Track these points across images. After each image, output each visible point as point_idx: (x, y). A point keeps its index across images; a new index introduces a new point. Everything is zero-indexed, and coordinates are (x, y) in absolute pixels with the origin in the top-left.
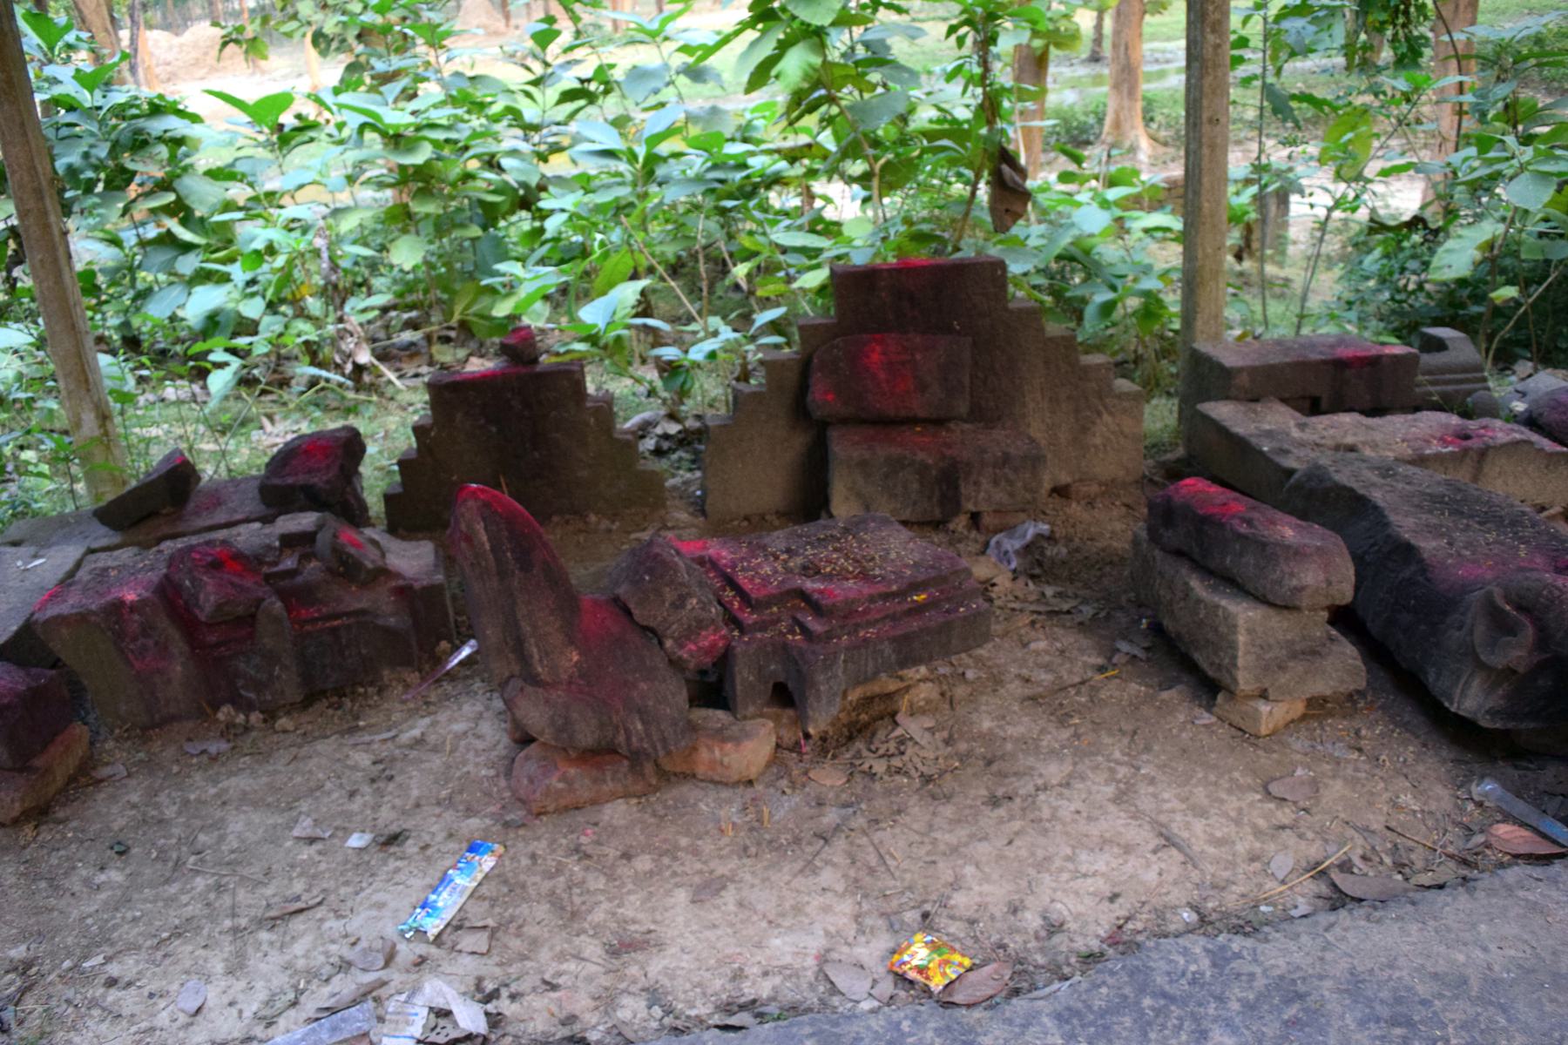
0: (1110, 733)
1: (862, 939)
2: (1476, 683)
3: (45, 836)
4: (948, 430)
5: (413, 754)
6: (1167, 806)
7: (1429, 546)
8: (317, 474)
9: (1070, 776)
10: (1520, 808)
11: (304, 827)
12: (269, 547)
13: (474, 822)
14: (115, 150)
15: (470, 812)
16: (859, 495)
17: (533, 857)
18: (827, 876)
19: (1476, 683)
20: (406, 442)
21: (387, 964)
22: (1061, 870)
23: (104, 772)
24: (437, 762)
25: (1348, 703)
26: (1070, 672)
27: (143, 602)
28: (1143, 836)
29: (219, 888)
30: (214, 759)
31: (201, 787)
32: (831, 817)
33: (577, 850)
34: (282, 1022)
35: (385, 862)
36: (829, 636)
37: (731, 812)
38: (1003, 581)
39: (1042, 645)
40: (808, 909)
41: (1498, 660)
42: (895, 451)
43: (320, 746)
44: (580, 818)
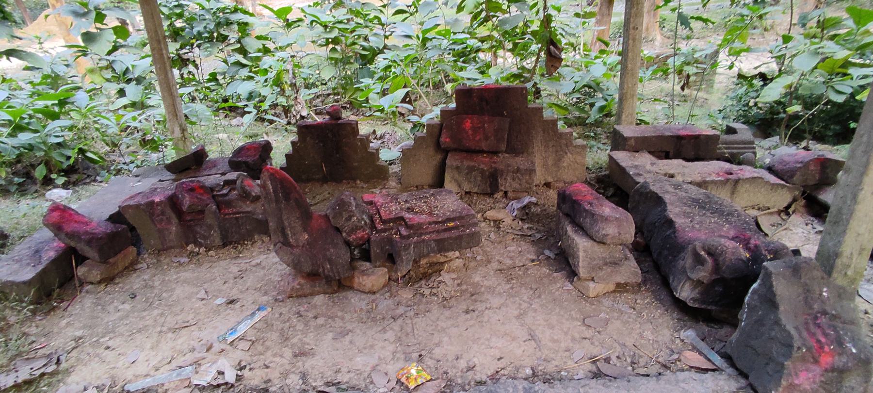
0: (526, 289)
1: (392, 362)
2: (687, 285)
3: (108, 289)
4: (498, 156)
5: (254, 269)
6: (538, 322)
7: (679, 221)
8: (252, 159)
9: (502, 304)
10: (702, 345)
11: (202, 294)
12: (218, 185)
13: (265, 298)
14: (218, 25)
15: (266, 294)
16: (456, 181)
17: (281, 314)
18: (390, 335)
19: (687, 285)
20: (289, 149)
21: (208, 350)
22: (482, 344)
23: (140, 266)
24: (262, 272)
25: (636, 288)
26: (520, 261)
27: (161, 202)
28: (523, 334)
29: (162, 315)
30: (181, 264)
31: (172, 275)
32: (401, 310)
33: (298, 313)
34: (162, 370)
35: (226, 310)
36: (408, 237)
37: (363, 305)
38: (508, 220)
39: (512, 248)
40: (376, 347)
41: (695, 276)
42: (472, 164)
43: (221, 263)
44: (304, 300)
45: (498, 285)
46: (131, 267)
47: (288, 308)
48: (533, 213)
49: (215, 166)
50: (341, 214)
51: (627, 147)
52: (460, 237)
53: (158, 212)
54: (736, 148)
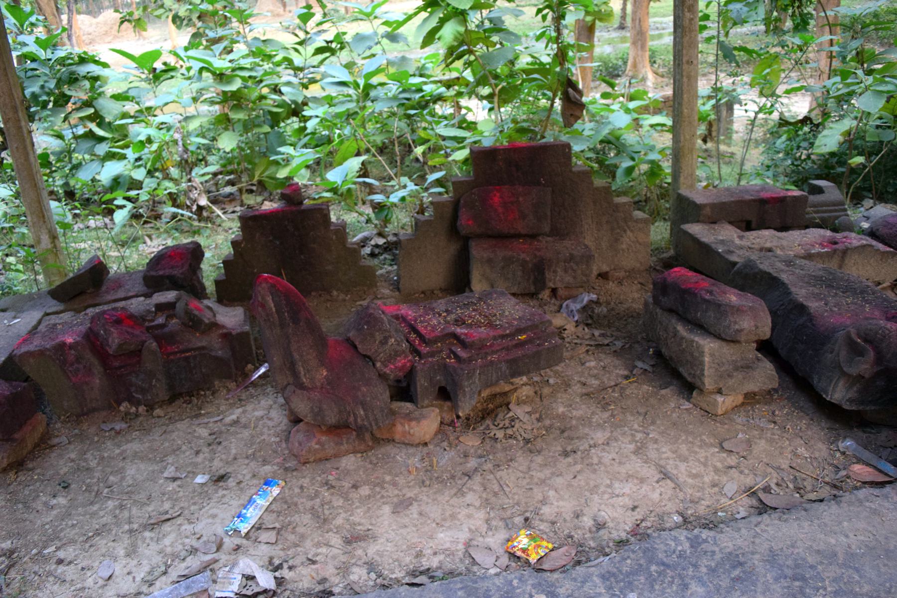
0: (633, 415)
1: (490, 533)
2: (841, 383)
4: (538, 241)
5: (232, 429)
6: (664, 456)
7: (813, 305)
8: (176, 269)
10: (866, 455)
11: (170, 472)
12: (149, 311)
13: (268, 468)
15: (265, 462)
16: (487, 279)
17: (302, 487)
18: (470, 497)
19: (841, 383)
20: (227, 250)
22: (604, 493)
23: (55, 441)
24: (246, 433)
25: (768, 396)
26: (609, 379)
28: (651, 472)
29: (121, 507)
30: (118, 433)
31: (111, 449)
32: (472, 463)
33: (327, 484)
35: (216, 492)
36: (470, 360)
37: (415, 461)
38: (570, 328)
39: (593, 364)
41: (853, 371)
43: (179, 425)
45: (593, 413)
46: (44, 444)
47: (307, 479)
48: (598, 315)
49: (120, 286)
50: (372, 336)
51: (702, 218)
52: (537, 354)
53: (71, 358)
54: (825, 212)
